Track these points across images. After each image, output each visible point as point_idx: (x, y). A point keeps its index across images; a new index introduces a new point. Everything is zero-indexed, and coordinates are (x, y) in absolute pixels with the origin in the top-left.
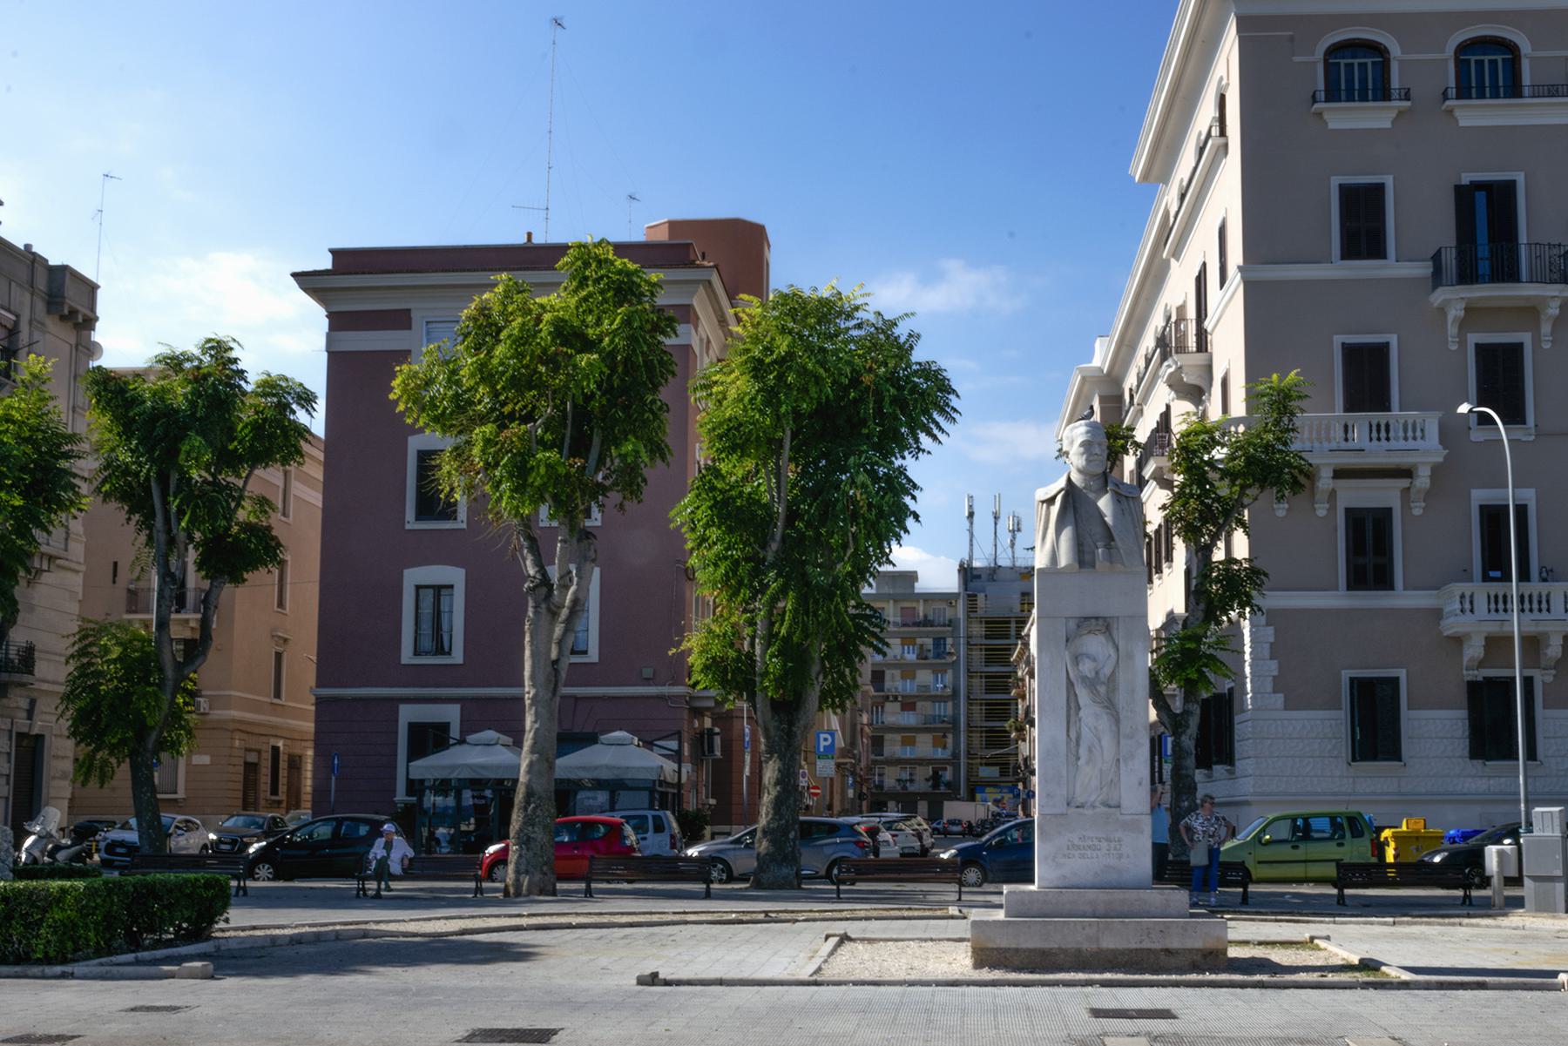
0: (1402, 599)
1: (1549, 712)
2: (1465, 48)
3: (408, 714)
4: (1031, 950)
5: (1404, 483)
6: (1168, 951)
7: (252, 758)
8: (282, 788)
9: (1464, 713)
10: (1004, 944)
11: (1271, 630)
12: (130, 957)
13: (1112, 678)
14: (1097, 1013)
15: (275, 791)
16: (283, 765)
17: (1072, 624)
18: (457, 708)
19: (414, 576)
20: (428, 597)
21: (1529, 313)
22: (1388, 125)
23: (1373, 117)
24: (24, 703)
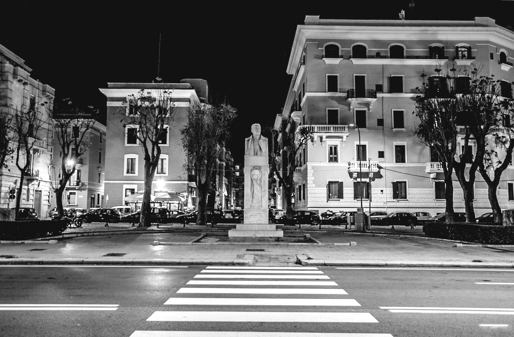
0: (406, 165)
1: (477, 189)
2: (327, 47)
3: (125, 187)
4: (241, 237)
5: (341, 140)
6: (270, 237)
7: (93, 196)
8: (100, 203)
9: (392, 189)
10: (236, 236)
11: (312, 170)
12: (40, 239)
13: (261, 179)
14: (263, 250)
15: (98, 203)
16: (100, 198)
17: (252, 167)
18: (136, 185)
19: (127, 156)
20: (130, 161)
21: (367, 105)
22: (507, 70)
23: (336, 61)
24: (37, 183)
